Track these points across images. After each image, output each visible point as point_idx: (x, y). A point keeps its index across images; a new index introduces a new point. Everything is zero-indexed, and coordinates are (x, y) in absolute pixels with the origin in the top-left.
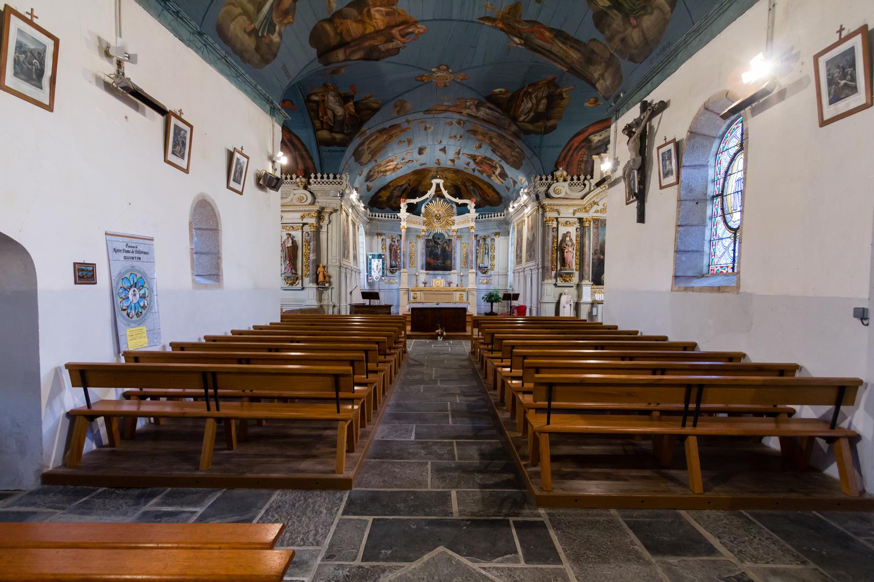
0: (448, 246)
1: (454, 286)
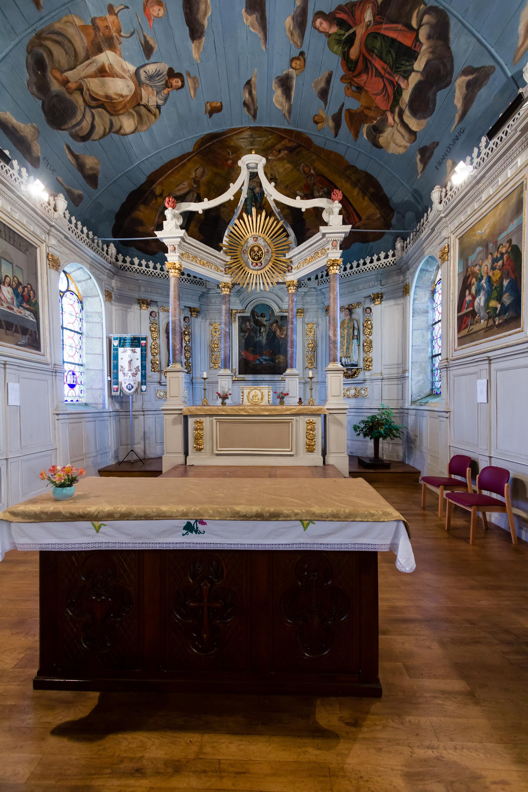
0: (281, 329)
1: (292, 401)
